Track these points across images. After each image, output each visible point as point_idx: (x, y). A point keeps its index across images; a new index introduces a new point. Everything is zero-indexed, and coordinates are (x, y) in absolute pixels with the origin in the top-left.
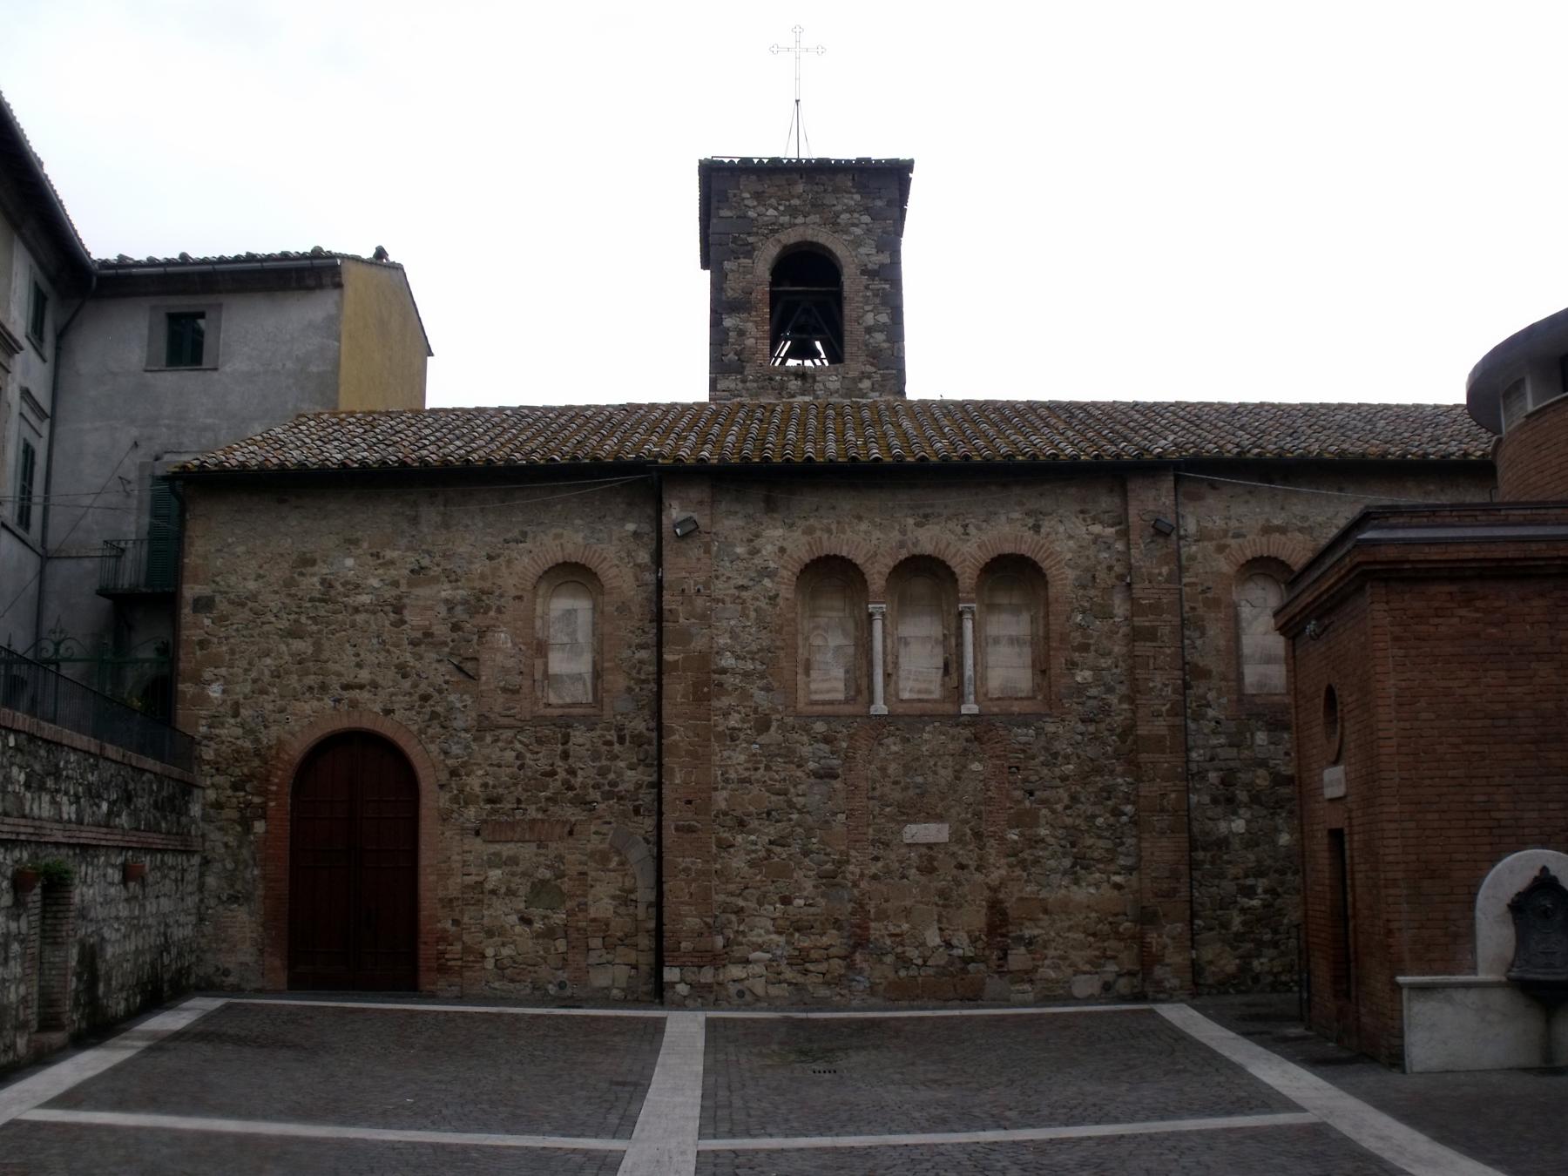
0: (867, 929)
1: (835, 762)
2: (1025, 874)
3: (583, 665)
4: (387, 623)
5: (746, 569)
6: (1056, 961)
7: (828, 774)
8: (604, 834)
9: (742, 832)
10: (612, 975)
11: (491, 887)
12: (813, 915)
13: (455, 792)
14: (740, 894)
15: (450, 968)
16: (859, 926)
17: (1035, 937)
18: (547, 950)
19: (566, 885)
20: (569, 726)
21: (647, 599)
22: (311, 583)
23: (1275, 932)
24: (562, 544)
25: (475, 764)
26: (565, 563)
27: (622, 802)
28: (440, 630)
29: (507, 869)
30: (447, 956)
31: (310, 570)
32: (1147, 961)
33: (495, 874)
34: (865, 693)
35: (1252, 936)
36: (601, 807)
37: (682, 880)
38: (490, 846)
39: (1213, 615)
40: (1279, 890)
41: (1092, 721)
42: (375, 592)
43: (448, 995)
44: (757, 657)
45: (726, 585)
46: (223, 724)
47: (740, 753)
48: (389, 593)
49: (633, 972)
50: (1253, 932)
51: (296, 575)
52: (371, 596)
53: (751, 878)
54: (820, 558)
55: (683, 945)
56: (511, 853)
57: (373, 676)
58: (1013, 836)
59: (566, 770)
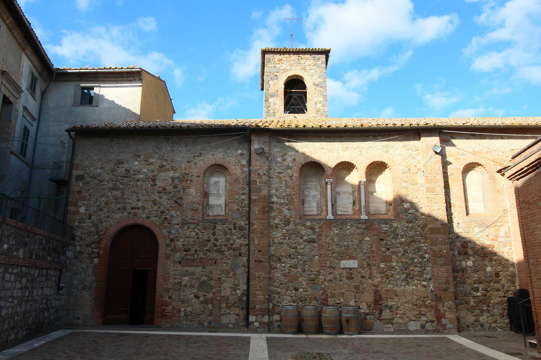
0: (327, 301)
1: (315, 236)
2: (388, 280)
3: (221, 201)
4: (149, 185)
5: (282, 166)
6: (401, 315)
7: (311, 241)
8: (228, 263)
9: (280, 263)
10: (229, 318)
13: (172, 247)
14: (279, 287)
15: (167, 316)
16: (324, 300)
17: (393, 306)
18: (205, 308)
19: (213, 283)
21: (245, 177)
22: (121, 170)
23: (488, 306)
24: (214, 158)
26: (216, 164)
28: (170, 188)
29: (191, 277)
30: (166, 311)
31: (122, 166)
32: (439, 316)
33: (186, 279)
35: (479, 307)
37: (257, 281)
39: (454, 184)
40: (488, 289)
41: (411, 222)
42: (145, 174)
43: (165, 326)
44: (285, 198)
45: (274, 172)
46: (84, 222)
47: (279, 233)
48: (151, 175)
49: (237, 317)
51: (116, 168)
52: (143, 175)
54: (308, 162)
55: (257, 306)
56: (192, 270)
57: (143, 205)
58: (382, 265)
59: (214, 239)
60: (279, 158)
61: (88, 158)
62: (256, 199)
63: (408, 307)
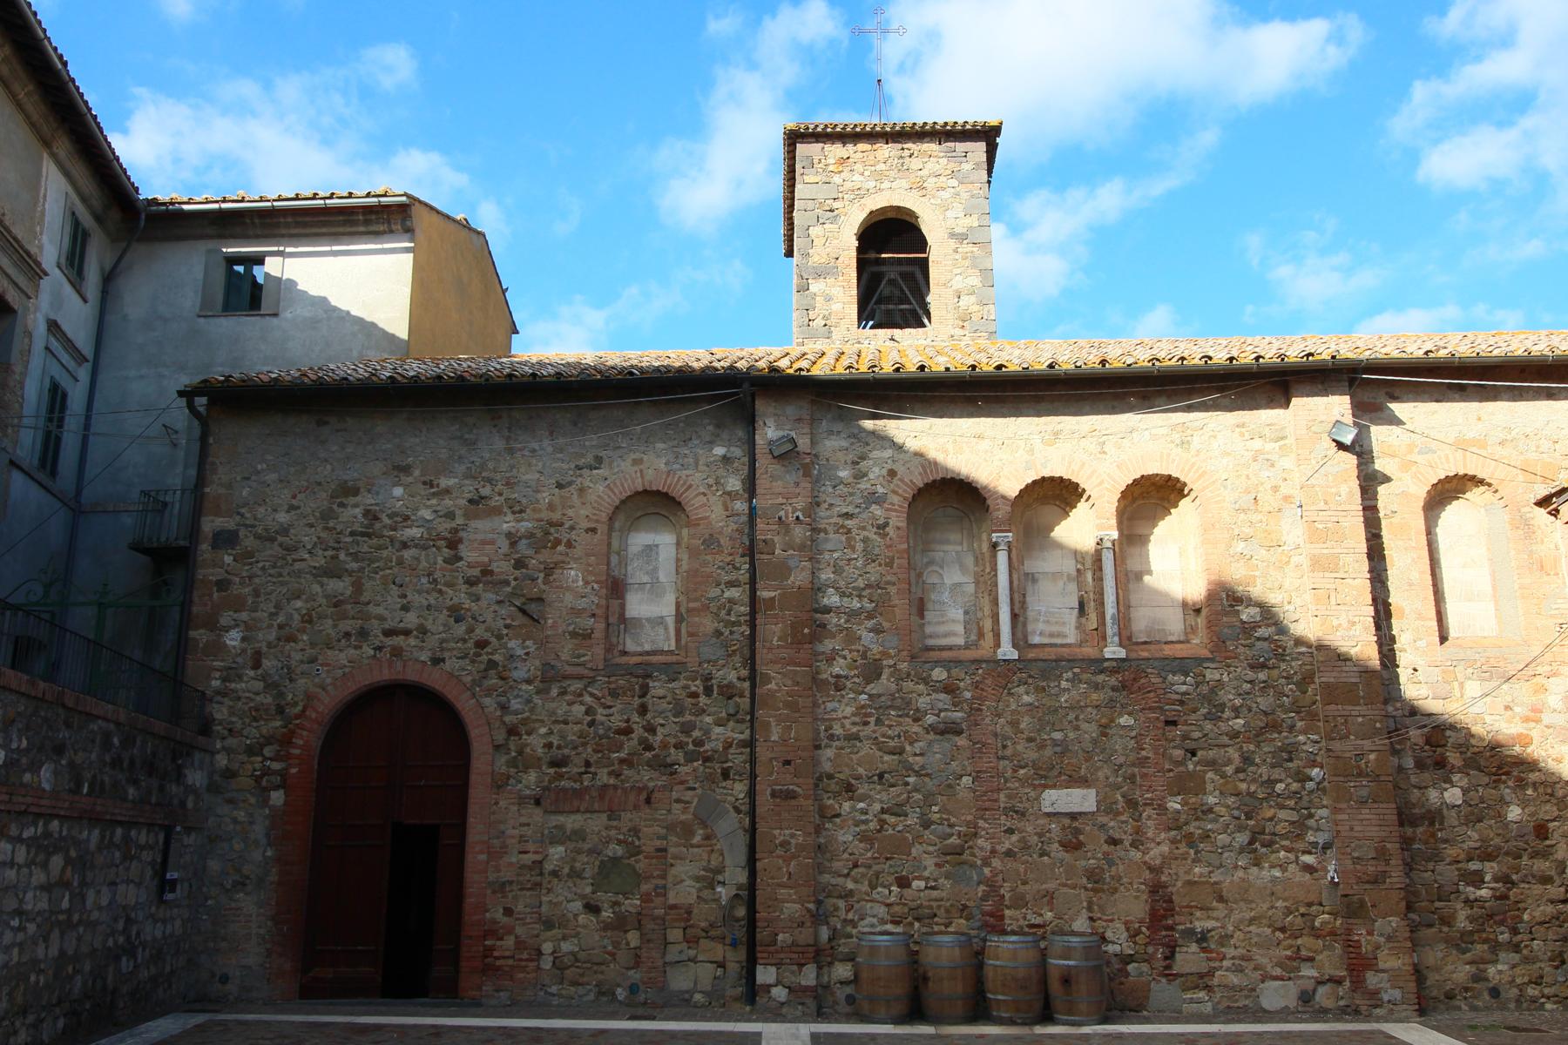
0: (1002, 917)
4: (440, 560)
5: (851, 494)
6: (1237, 962)
7: (949, 730)
8: (688, 802)
9: (851, 799)
11: (552, 867)
12: (936, 900)
15: (498, 968)
16: (991, 914)
17: (1209, 931)
18: (616, 945)
19: (641, 865)
20: (649, 676)
22: (352, 514)
24: (641, 471)
25: (537, 720)
26: (645, 492)
27: (707, 764)
28: (502, 567)
29: (572, 845)
31: (352, 500)
32: (1359, 965)
33: (557, 852)
34: (989, 636)
36: (683, 770)
37: (778, 857)
38: (553, 817)
40: (1514, 877)
41: (1263, 666)
42: (427, 525)
44: (864, 593)
48: (444, 526)
49: (720, 972)
50: (1484, 930)
52: (422, 530)
53: (861, 855)
54: (934, 481)
55: (780, 937)
56: (577, 826)
58: (1174, 804)
60: (845, 469)
61: (248, 479)
62: (773, 599)
63: (1258, 935)
